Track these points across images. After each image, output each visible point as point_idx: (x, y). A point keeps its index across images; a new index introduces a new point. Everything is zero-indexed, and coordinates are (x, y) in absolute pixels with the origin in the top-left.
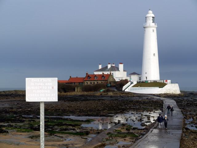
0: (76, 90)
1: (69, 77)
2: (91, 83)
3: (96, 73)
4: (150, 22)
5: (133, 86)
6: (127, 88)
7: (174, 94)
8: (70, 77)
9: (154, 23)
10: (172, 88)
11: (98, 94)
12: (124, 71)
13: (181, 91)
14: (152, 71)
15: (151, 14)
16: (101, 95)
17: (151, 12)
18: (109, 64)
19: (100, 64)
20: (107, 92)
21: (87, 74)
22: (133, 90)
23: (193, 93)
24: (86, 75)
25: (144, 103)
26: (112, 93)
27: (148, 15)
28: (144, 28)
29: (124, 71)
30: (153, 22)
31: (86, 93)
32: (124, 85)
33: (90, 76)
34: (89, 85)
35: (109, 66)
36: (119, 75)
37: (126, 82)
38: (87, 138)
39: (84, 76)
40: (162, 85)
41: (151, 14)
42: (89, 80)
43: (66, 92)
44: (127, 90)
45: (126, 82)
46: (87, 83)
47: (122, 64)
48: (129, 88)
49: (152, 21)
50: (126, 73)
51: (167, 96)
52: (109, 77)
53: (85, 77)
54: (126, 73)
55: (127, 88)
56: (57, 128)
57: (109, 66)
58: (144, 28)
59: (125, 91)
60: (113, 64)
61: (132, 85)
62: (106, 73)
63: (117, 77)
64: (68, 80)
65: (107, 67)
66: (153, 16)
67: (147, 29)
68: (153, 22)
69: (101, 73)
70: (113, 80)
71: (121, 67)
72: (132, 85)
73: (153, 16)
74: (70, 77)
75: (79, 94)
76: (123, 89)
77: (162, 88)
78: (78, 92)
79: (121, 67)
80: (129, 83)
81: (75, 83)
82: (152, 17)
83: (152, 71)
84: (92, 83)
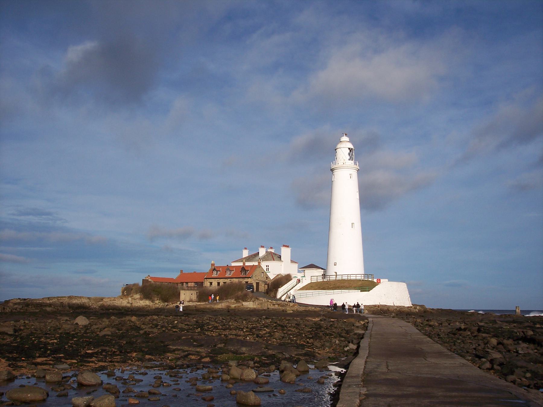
2: (219, 283)
5: (302, 289)
7: (398, 307)
8: (182, 271)
9: (353, 162)
10: (392, 294)
12: (292, 261)
14: (347, 255)
18: (262, 247)
19: (246, 249)
23: (277, 278)
29: (292, 261)
30: (349, 160)
35: (262, 252)
38: (178, 381)
40: (365, 286)
41: (345, 146)
45: (287, 278)
46: (211, 283)
47: (288, 247)
49: (349, 157)
51: (381, 311)
57: (262, 252)
60: (271, 248)
66: (349, 147)
67: (336, 173)
68: (349, 160)
70: (265, 279)
71: (286, 253)
72: (300, 285)
73: (351, 146)
76: (278, 296)
77: (369, 291)
82: (349, 149)
83: (347, 255)
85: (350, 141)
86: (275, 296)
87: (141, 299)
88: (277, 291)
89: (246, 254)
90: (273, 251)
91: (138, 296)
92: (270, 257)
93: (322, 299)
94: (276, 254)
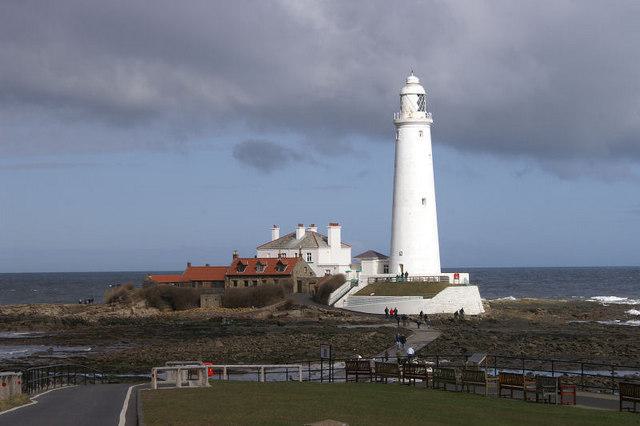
0: (203, 302)
3: (262, 254)
4: (411, 102)
5: (359, 293)
6: (340, 299)
11: (262, 314)
15: (414, 89)
16: (271, 317)
17: (413, 79)
18: (301, 225)
20: (287, 309)
21: (235, 256)
22: (357, 302)
26: (299, 312)
27: (405, 90)
28: (402, 95)
29: (344, 244)
31: (229, 312)
32: (332, 290)
33: (244, 264)
35: (301, 233)
39: (228, 262)
41: (414, 89)
43: (174, 310)
44: (339, 305)
45: (339, 280)
46: (235, 283)
48: (345, 297)
49: (417, 107)
50: (348, 252)
52: (292, 267)
53: (229, 265)
54: (348, 252)
55: (340, 299)
58: (402, 95)
59: (336, 305)
60: (313, 226)
62: (291, 254)
63: (320, 263)
65: (294, 236)
66: (420, 93)
69: (274, 254)
71: (335, 234)
72: (356, 289)
78: (210, 307)
79: (335, 234)
80: (347, 285)
81: (200, 282)
84: (250, 283)
86: (326, 304)
88: (328, 296)
89: (276, 235)
90: (314, 230)
91: (142, 304)
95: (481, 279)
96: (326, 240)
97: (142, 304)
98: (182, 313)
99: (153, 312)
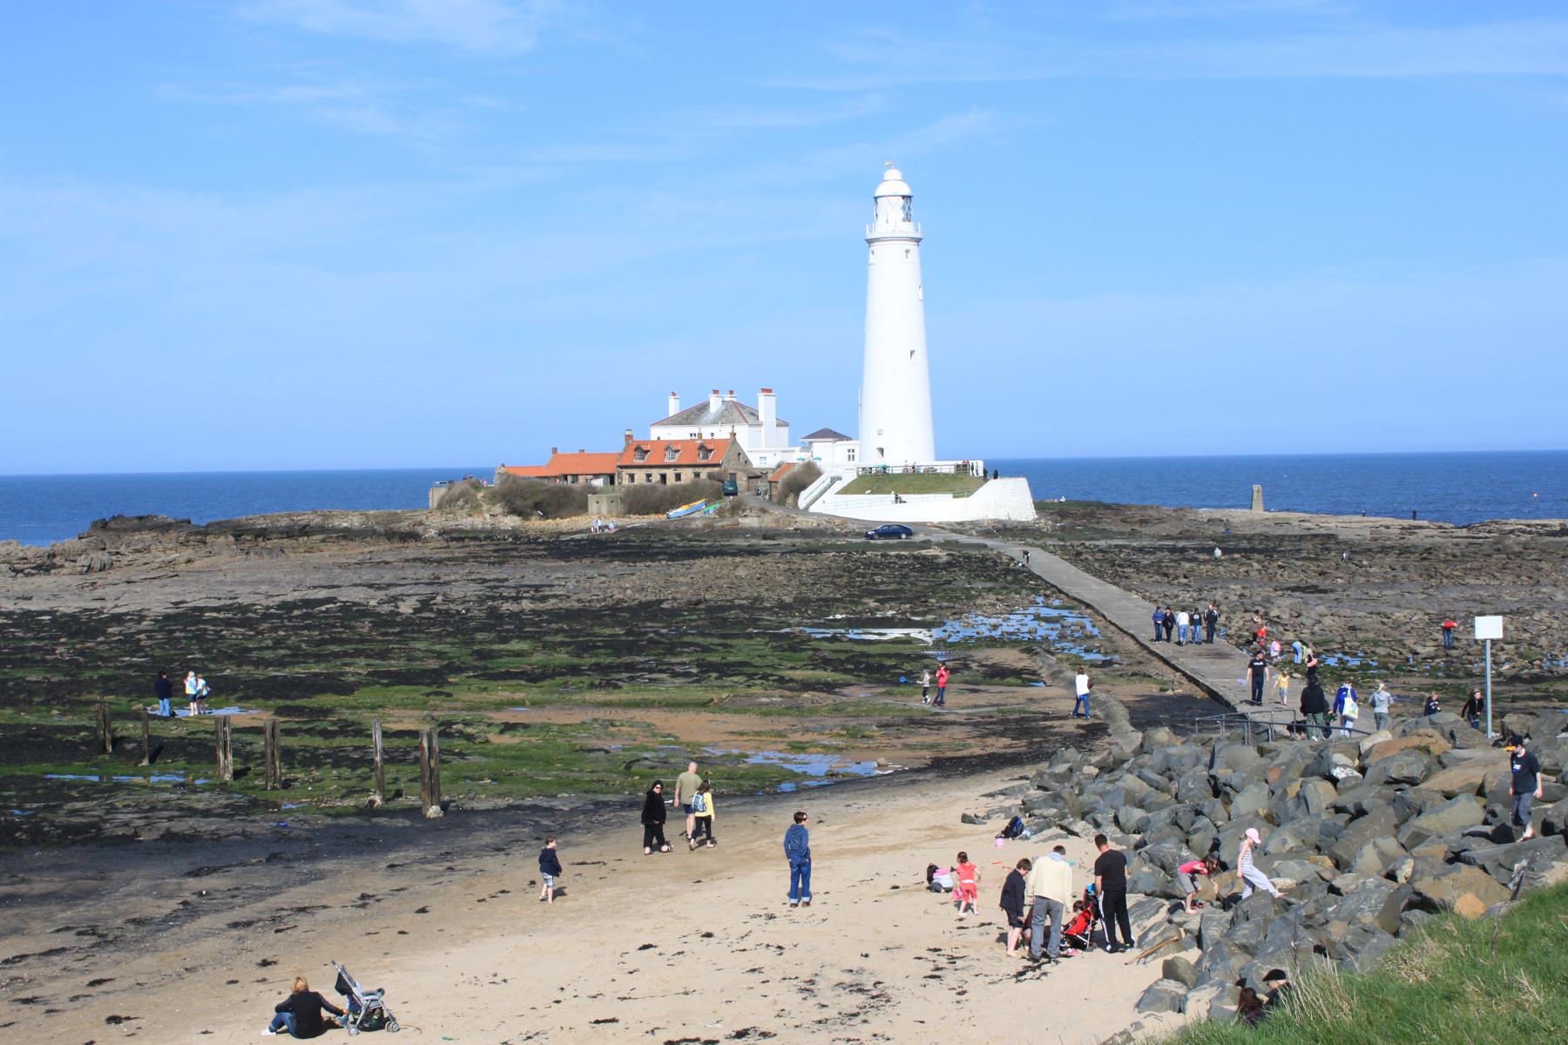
0: (592, 507)
1: (550, 455)
4: (890, 219)
6: (828, 503)
8: (555, 450)
13: (1040, 507)
21: (629, 437)
24: (623, 444)
25: (297, 660)
28: (870, 242)
29: (781, 424)
32: (804, 487)
34: (653, 488)
35: (715, 405)
36: (765, 447)
37: (810, 472)
40: (960, 481)
41: (893, 184)
42: (640, 462)
45: (810, 472)
46: (632, 477)
49: (902, 215)
56: (989, 563)
57: (715, 405)
58: (870, 242)
59: (812, 509)
61: (839, 486)
64: (549, 466)
65: (704, 407)
71: (766, 407)
72: (839, 486)
73: (907, 192)
74: (555, 450)
75: (613, 524)
78: (600, 518)
81: (575, 476)
84: (671, 480)
85: (905, 179)
87: (505, 514)
88: (797, 495)
89: (674, 408)
92: (736, 414)
93: (879, 509)
94: (744, 407)
95: (1038, 474)
96: (754, 414)
97: (498, 509)
98: (565, 524)
99: (511, 522)
